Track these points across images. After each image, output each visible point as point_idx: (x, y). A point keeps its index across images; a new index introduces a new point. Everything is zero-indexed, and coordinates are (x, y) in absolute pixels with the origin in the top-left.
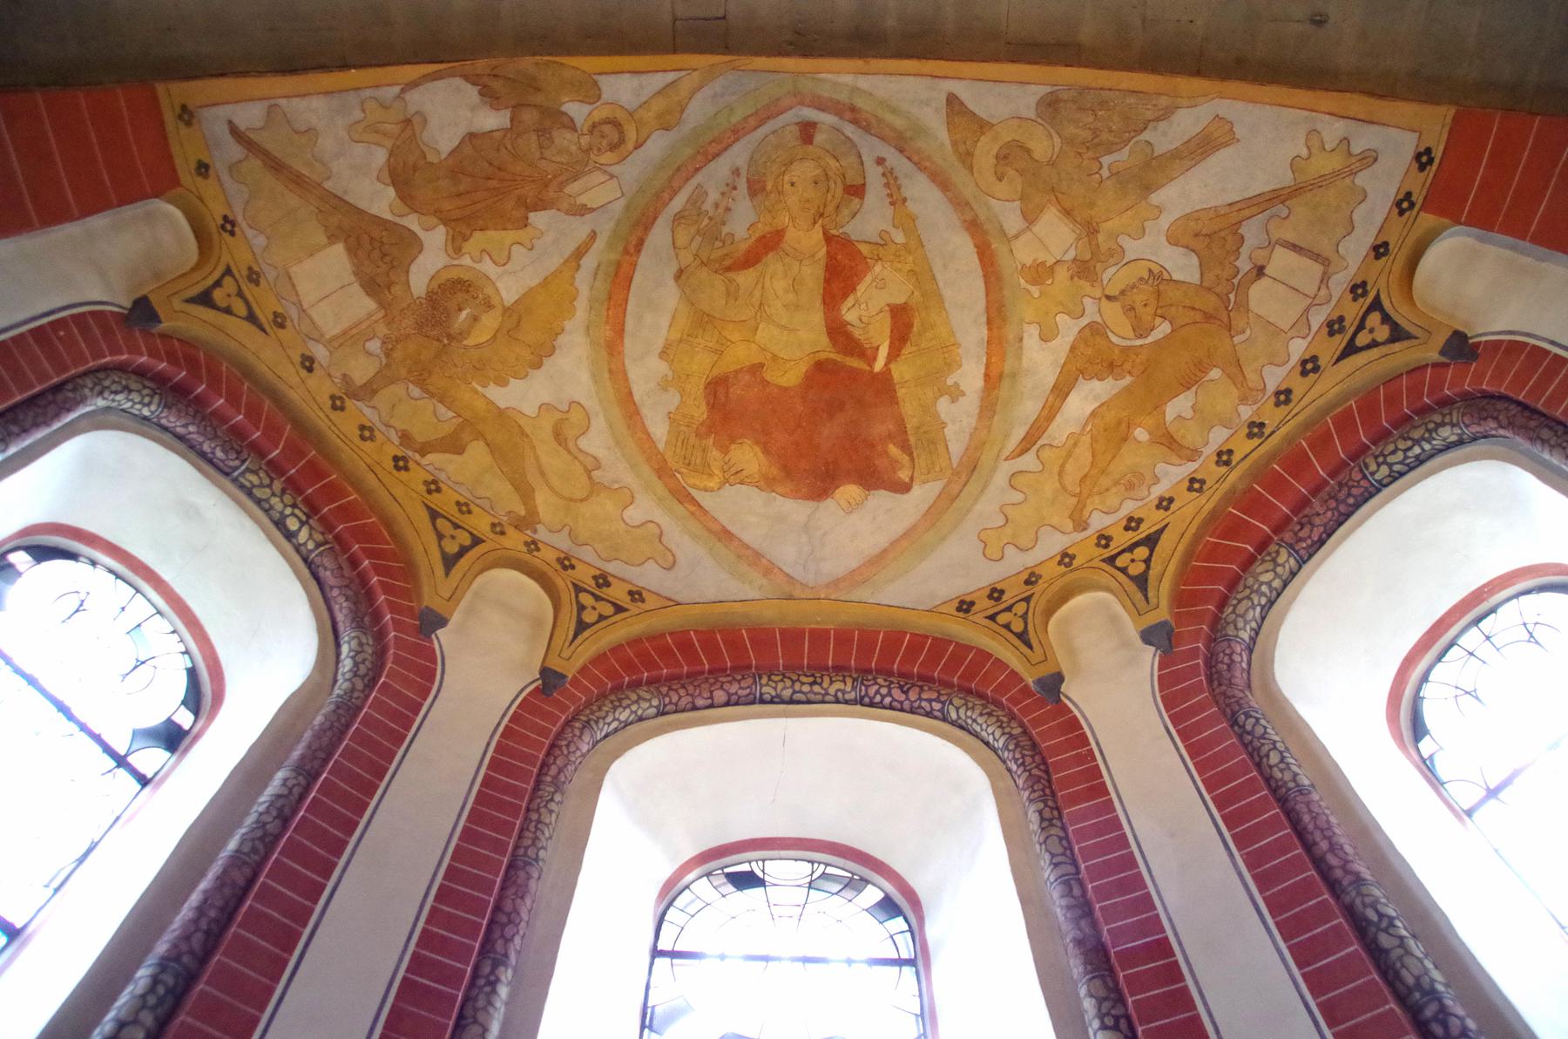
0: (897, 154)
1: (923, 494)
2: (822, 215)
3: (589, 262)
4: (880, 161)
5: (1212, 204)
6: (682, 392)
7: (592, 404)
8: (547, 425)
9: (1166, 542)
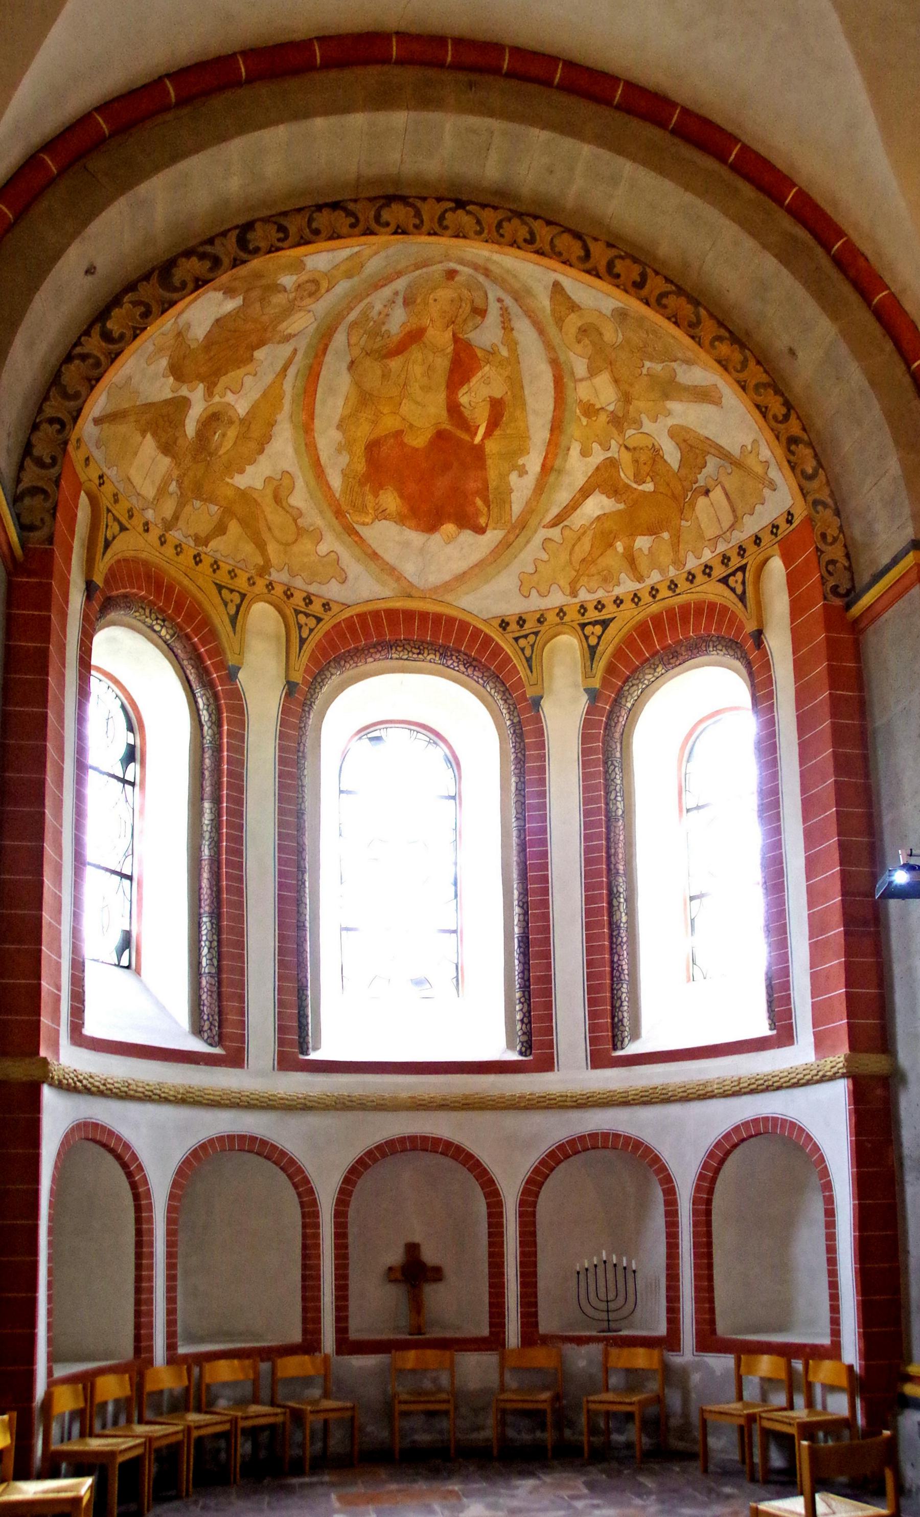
1: (493, 536)
2: (453, 322)
3: (292, 371)
4: (499, 300)
6: (351, 453)
7: (294, 469)
8: (269, 492)
9: (612, 628)
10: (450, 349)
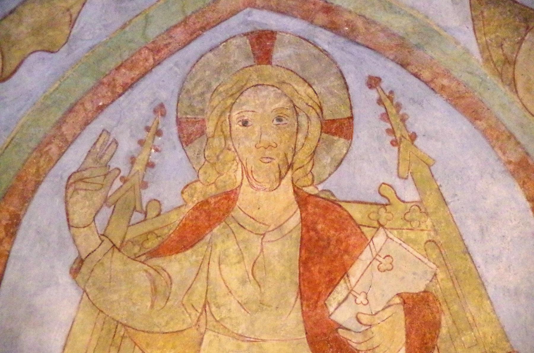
0: (397, 68)
2: (290, 166)
4: (373, 82)
10: (295, 220)
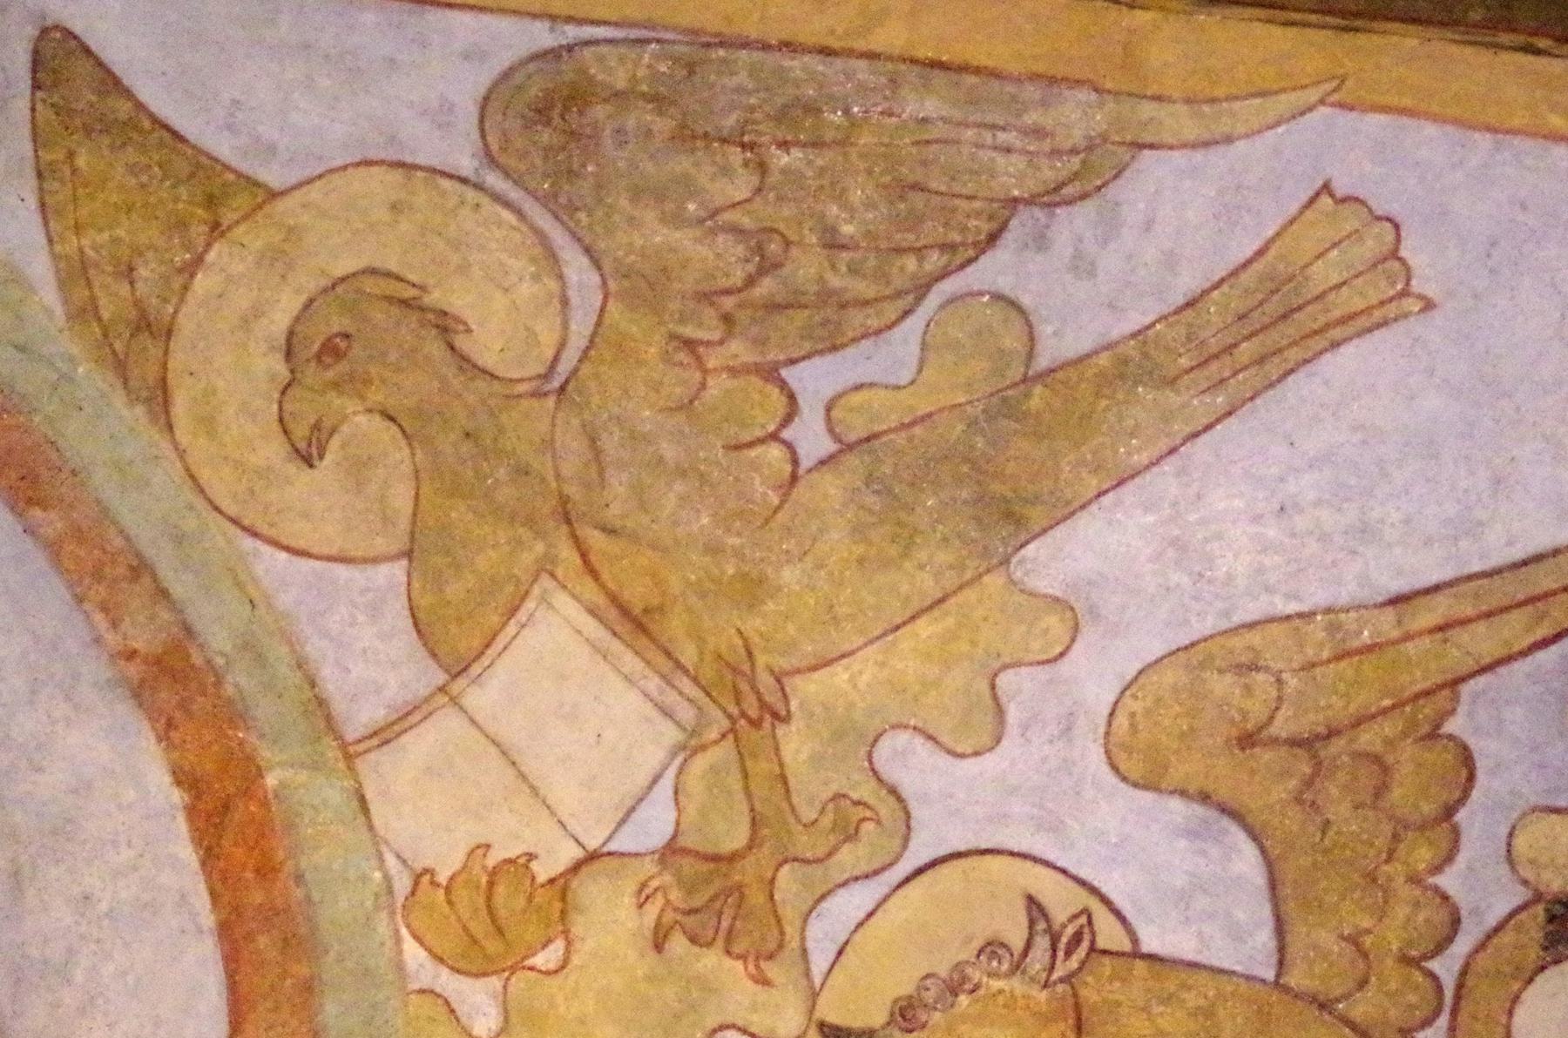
5: (1316, 595)
